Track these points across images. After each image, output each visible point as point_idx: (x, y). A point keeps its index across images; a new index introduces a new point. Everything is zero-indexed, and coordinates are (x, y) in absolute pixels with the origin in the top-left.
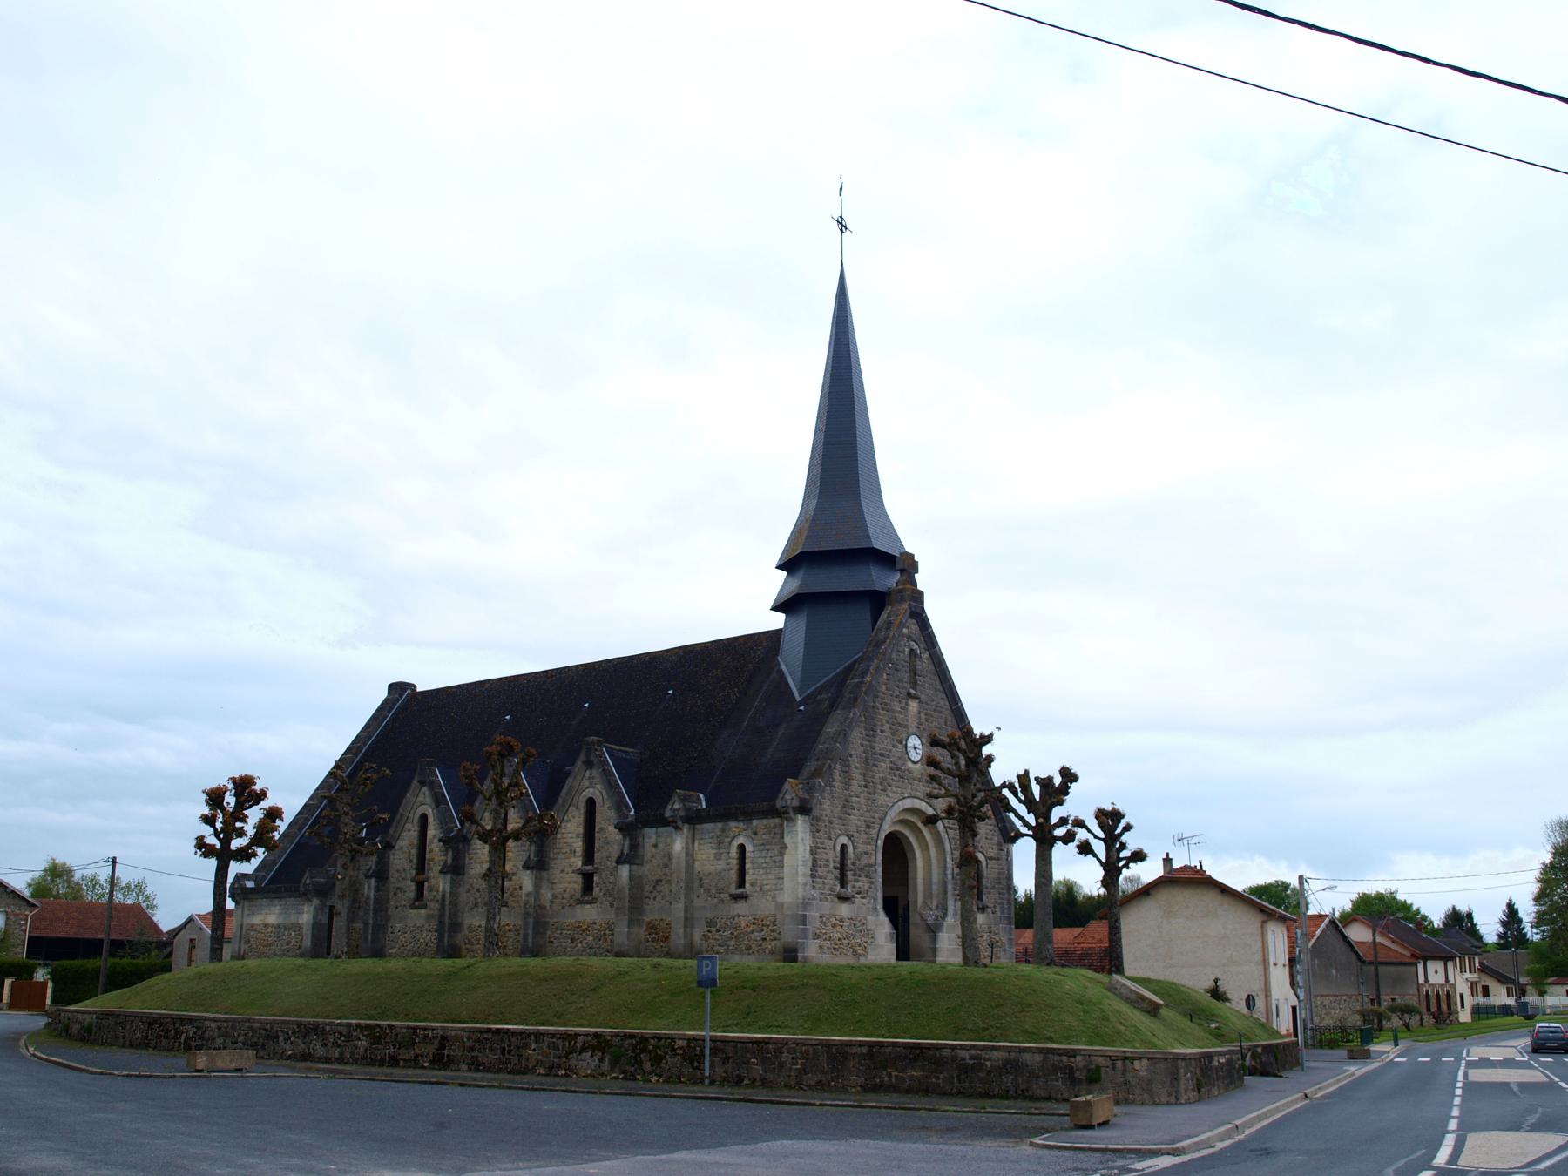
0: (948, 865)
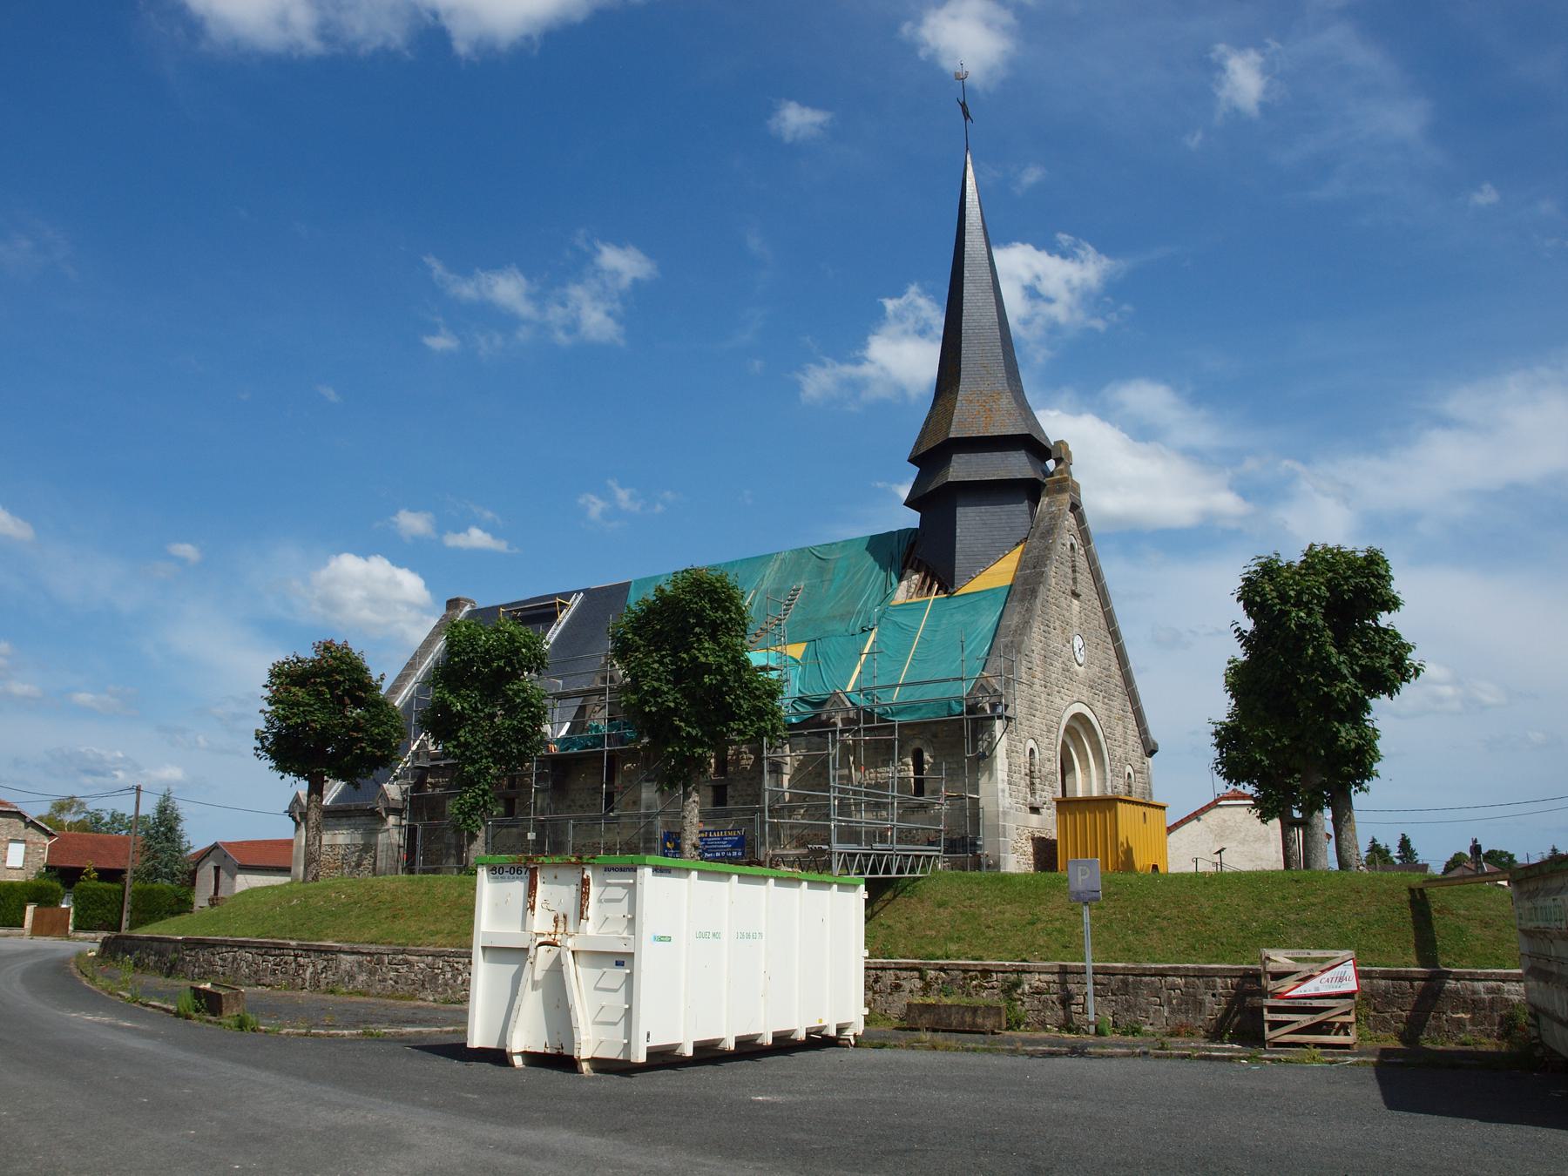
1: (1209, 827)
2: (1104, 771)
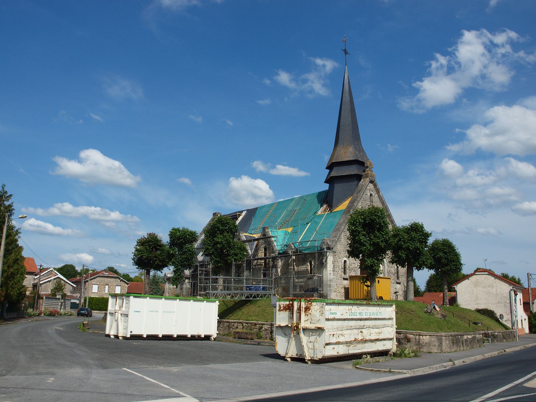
1: (472, 282)
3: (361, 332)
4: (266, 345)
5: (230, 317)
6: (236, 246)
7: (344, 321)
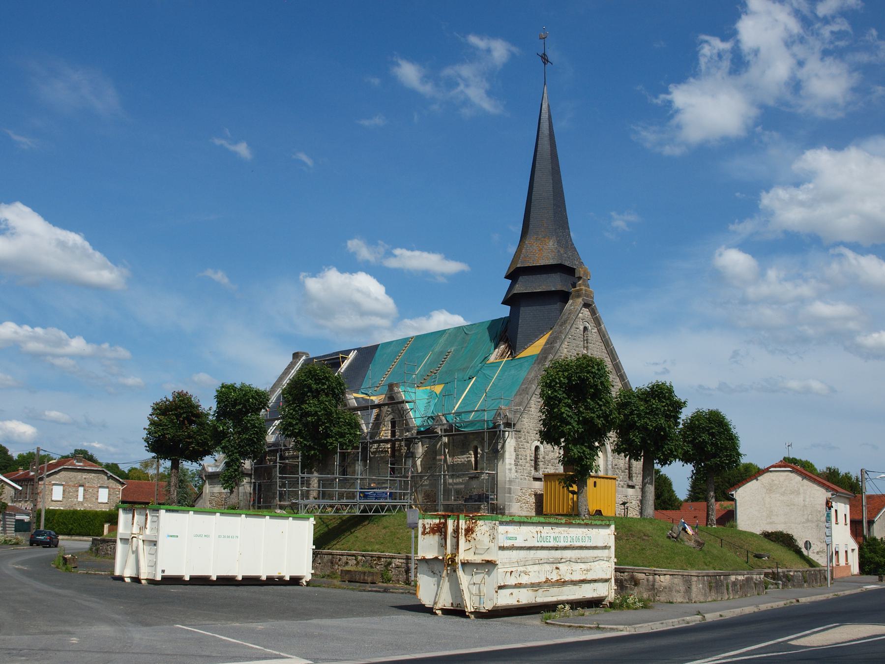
0: (609, 459)
1: (763, 485)
2: (607, 456)
3: (557, 568)
4: (399, 593)
5: (333, 545)
6: (341, 420)
7: (528, 551)
